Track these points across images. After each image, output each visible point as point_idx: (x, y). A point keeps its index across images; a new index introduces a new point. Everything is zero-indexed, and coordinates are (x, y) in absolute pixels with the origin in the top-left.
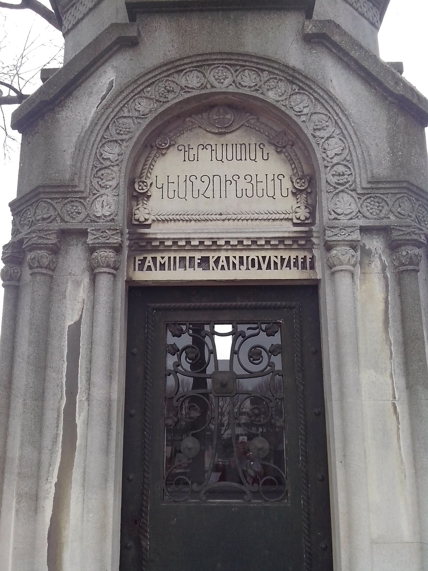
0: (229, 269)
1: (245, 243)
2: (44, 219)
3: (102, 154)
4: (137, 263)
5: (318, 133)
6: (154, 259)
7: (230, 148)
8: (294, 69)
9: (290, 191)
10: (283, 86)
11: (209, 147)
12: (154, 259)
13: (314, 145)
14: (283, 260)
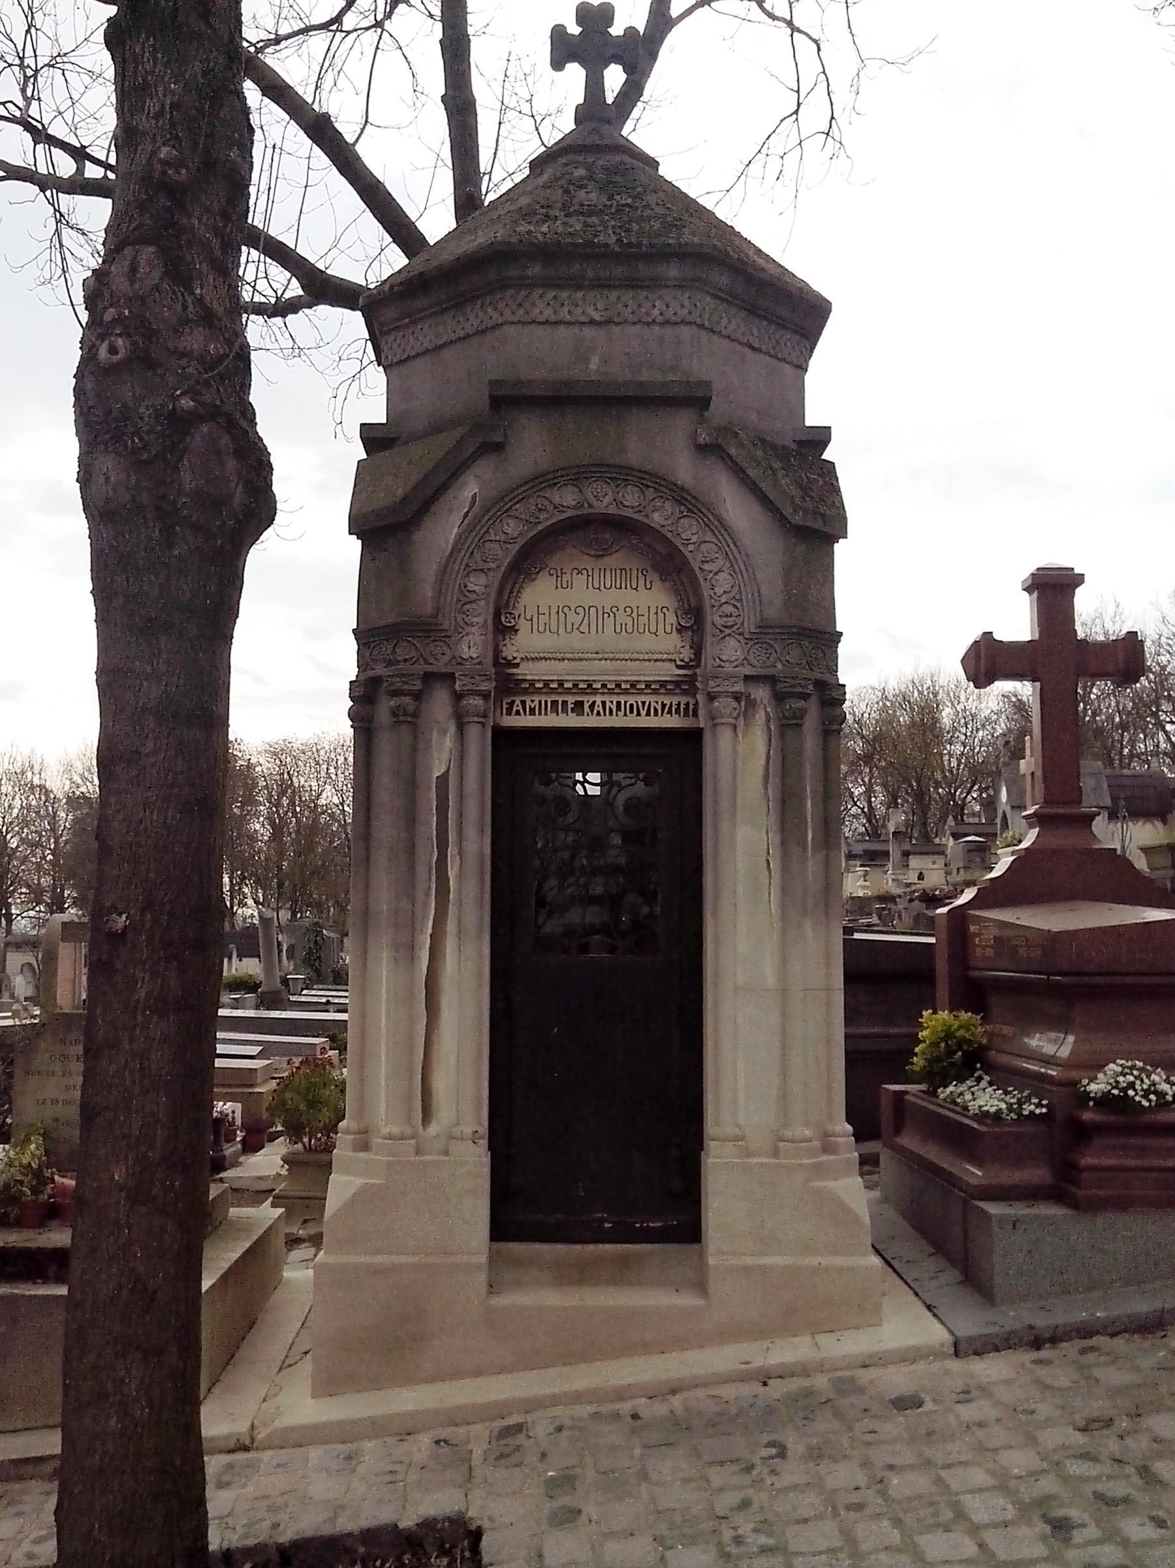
0: (605, 715)
1: (623, 686)
2: (405, 660)
3: (466, 586)
4: (505, 707)
5: (706, 567)
6: (523, 703)
7: (608, 573)
8: (683, 489)
9: (674, 627)
10: (669, 507)
11: (584, 572)
12: (523, 703)
13: (701, 580)
14: (664, 705)
